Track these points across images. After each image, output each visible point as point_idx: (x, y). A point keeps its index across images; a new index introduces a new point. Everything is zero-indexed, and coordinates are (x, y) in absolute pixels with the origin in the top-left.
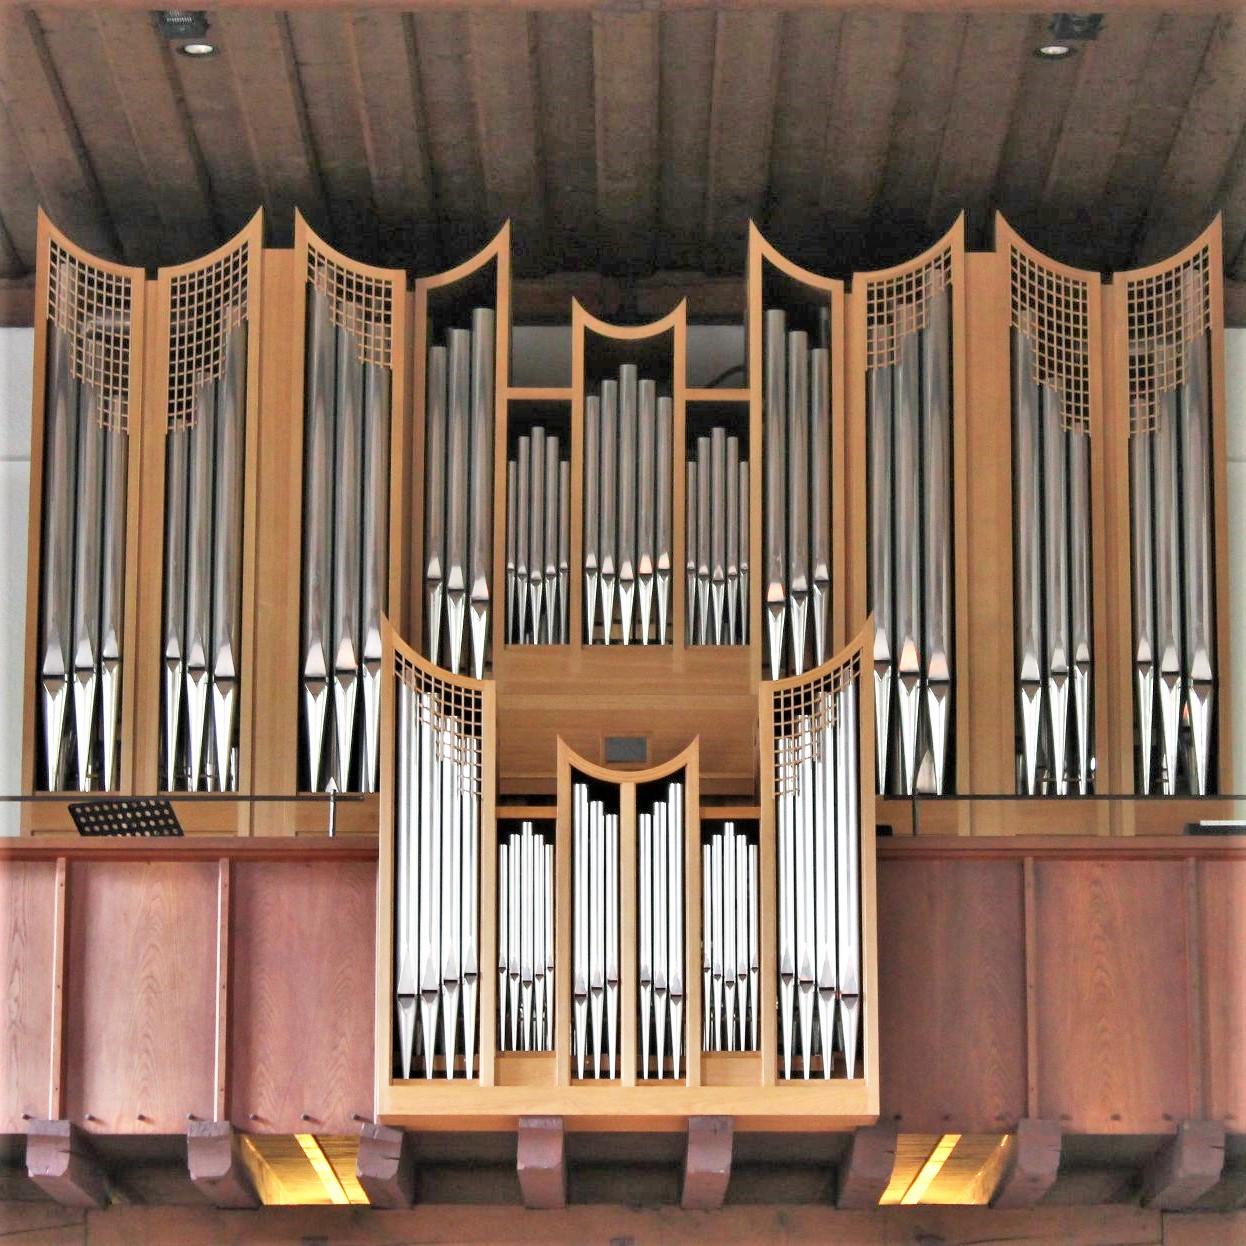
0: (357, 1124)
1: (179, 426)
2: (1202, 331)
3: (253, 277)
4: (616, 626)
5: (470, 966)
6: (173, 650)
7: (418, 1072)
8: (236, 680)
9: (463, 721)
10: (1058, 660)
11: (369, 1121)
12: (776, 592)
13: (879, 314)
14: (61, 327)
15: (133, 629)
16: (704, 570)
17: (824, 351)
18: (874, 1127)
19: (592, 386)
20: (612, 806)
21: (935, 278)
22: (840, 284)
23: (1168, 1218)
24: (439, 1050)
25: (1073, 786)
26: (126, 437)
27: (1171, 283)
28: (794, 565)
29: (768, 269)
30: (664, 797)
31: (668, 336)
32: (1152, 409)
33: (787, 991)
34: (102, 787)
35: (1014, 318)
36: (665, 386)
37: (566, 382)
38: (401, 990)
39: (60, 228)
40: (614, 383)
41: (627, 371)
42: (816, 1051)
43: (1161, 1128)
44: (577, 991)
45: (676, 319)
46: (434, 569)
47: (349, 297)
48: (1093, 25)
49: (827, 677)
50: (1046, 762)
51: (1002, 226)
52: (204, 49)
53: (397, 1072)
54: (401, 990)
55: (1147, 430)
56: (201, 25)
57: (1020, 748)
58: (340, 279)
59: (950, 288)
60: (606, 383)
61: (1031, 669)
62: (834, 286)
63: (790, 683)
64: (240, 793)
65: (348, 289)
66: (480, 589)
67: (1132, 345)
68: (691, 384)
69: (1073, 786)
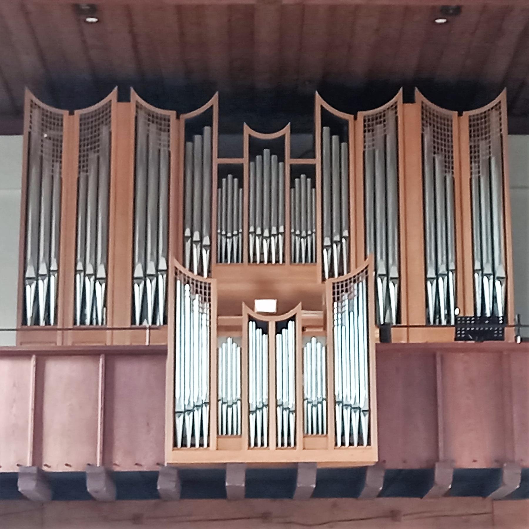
0: (158, 466)
1: (83, 175)
2: (499, 135)
3: (113, 114)
4: (262, 256)
5: (204, 398)
6: (80, 267)
7: (184, 445)
8: (106, 279)
9: (203, 296)
10: (442, 269)
11: (163, 465)
12: (327, 242)
13: (368, 128)
14: (34, 135)
15: (464, 214)
16: (298, 232)
17: (346, 144)
18: (374, 466)
19: (252, 158)
20: (265, 332)
21: (390, 114)
22: (352, 116)
23: (495, 502)
24: (193, 435)
25: (449, 322)
26: (61, 179)
27: (486, 115)
28: (334, 231)
29: (323, 110)
30: (286, 328)
31: (283, 137)
32: (479, 167)
33: (338, 408)
34: (50, 325)
35: (423, 130)
36: (281, 159)
37: (242, 156)
38: (177, 410)
39: (35, 95)
40: (260, 156)
41: (266, 151)
42: (351, 434)
43: (494, 466)
44: (251, 410)
45: (286, 131)
46: (188, 233)
47: (153, 122)
48: (458, 10)
49: (354, 277)
50: (437, 311)
51: (417, 93)
52: (94, 20)
53: (175, 445)
54: (177, 410)
55: (477, 175)
56: (93, 10)
57: (427, 306)
58: (149, 115)
59: (397, 118)
60: (258, 157)
61: (431, 274)
62: (348, 117)
63: (342, 278)
64: (108, 327)
65: (152, 118)
66: (206, 241)
67: (470, 141)
68: (292, 156)
69: (449, 322)
